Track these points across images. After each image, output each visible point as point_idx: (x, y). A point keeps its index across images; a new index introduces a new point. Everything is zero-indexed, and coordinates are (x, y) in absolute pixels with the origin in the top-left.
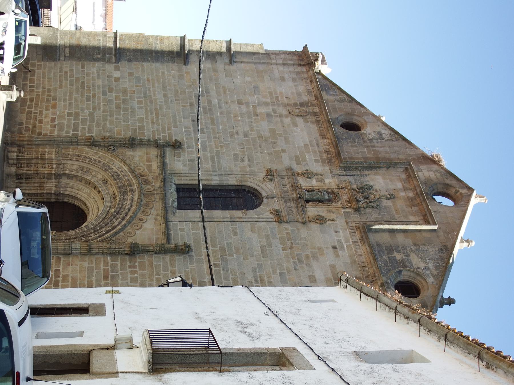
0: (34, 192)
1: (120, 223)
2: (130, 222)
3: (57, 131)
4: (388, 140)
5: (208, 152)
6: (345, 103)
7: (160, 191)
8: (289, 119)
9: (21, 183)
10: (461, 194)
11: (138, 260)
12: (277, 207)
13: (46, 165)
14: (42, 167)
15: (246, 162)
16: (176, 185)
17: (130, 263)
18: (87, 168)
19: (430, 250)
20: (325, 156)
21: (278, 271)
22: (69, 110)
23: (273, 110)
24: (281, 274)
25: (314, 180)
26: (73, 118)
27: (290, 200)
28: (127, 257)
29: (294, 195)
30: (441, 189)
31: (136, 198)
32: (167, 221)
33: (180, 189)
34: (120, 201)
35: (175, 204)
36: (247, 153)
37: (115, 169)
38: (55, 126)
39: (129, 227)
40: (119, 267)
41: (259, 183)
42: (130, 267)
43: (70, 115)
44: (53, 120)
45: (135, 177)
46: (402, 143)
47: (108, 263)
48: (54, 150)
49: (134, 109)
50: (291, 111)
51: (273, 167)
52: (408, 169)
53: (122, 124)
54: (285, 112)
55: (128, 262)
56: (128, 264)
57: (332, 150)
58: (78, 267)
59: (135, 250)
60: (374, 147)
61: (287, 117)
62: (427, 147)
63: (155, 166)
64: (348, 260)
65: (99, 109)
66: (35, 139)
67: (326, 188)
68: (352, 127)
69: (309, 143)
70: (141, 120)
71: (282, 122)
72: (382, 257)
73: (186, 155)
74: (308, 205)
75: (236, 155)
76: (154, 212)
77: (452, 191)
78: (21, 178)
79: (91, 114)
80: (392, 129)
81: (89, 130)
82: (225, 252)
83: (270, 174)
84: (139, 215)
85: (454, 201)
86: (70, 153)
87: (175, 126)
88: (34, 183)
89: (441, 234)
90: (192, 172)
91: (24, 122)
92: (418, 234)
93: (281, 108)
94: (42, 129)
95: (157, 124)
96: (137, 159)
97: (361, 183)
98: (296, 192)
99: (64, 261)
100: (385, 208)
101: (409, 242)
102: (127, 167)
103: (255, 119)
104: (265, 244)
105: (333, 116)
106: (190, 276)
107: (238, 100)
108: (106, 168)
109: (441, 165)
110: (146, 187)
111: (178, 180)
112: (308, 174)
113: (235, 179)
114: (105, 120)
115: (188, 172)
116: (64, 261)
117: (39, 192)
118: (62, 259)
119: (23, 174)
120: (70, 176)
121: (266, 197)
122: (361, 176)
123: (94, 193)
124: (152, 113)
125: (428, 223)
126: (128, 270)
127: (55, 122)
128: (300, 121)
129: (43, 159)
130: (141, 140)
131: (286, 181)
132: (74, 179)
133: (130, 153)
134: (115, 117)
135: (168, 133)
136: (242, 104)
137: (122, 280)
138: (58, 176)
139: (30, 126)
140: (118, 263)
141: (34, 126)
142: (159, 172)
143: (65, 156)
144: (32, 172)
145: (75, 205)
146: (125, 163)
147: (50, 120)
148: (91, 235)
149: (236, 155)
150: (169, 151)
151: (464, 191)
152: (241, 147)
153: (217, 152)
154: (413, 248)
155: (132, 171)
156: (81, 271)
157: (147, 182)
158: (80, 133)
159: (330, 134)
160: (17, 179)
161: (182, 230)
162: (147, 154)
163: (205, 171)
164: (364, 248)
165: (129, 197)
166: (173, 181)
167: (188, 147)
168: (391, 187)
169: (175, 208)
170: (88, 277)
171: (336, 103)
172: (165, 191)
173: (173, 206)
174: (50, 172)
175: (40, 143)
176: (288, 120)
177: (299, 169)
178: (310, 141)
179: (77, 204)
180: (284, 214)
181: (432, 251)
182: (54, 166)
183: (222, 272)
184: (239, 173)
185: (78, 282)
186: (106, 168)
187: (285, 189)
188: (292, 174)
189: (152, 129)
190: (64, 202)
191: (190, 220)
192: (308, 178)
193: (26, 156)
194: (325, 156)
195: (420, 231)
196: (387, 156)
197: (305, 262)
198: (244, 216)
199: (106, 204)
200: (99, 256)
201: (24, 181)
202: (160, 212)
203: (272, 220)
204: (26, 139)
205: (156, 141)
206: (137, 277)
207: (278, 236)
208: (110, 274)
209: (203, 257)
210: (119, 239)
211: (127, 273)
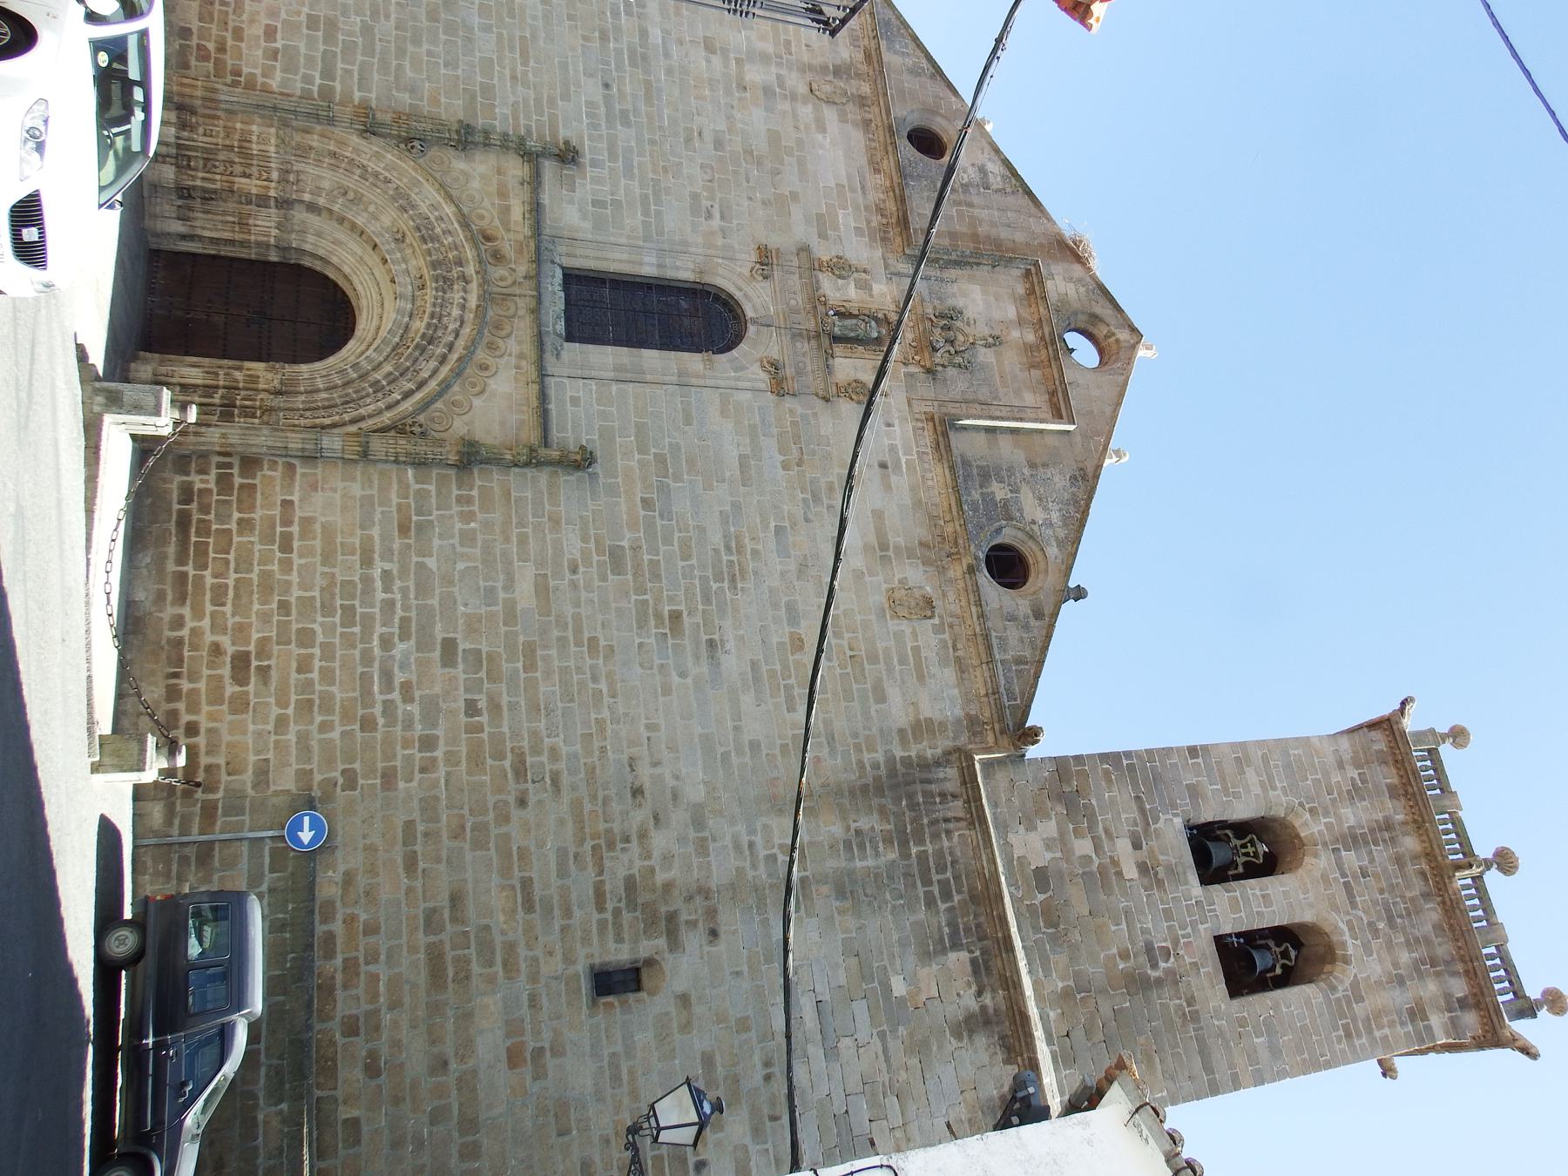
0: (226, 235)
1: (435, 372)
2: (458, 373)
3: (283, 71)
4: (997, 191)
5: (636, 183)
6: (924, 79)
7: (527, 289)
8: (810, 108)
9: (191, 209)
10: (1117, 341)
11: (478, 483)
12: (774, 353)
13: (254, 170)
14: (245, 175)
15: (716, 222)
16: (563, 268)
17: (459, 488)
18: (356, 192)
19: (1056, 479)
20: (876, 220)
21: (772, 524)
22: (311, 7)
23: (779, 77)
24: (779, 531)
25: (852, 285)
26: (320, 34)
27: (801, 335)
28: (452, 472)
29: (811, 325)
30: (1082, 321)
31: (473, 302)
32: (542, 375)
33: (573, 279)
34: (434, 305)
35: (561, 326)
36: (719, 195)
37: (424, 208)
38: (274, 55)
39: (456, 388)
40: (433, 500)
41: (740, 283)
42: (459, 500)
43: (313, 22)
44: (270, 33)
45: (472, 240)
46: (1024, 201)
47: (408, 486)
48: (273, 130)
49: (470, 29)
50: (815, 86)
51: (774, 241)
52: (1033, 277)
53: (443, 71)
54: (802, 89)
55: (454, 487)
56: (455, 492)
57: (891, 206)
58: (338, 496)
59: (471, 458)
60: (970, 205)
61: (805, 102)
62: (1067, 217)
63: (518, 211)
64: (908, 501)
65: (387, 17)
66: (223, 97)
67: (874, 307)
68: (927, 142)
69: (845, 183)
70: (487, 65)
71: (795, 115)
72: (969, 494)
73: (587, 185)
74: (839, 349)
75: (695, 197)
76: (512, 346)
77: (1100, 332)
78: (190, 196)
79: (367, 30)
80: (1007, 164)
81: (361, 79)
82: (666, 468)
83: (766, 260)
84: (481, 355)
85: (1101, 352)
86: (315, 144)
87: (566, 96)
88: (224, 213)
89: (1078, 439)
90: (600, 238)
91: (195, 30)
92: (1036, 437)
93: (794, 75)
94: (240, 58)
95: (526, 84)
96: (476, 184)
97: (940, 299)
98: (815, 317)
99: (303, 475)
100: (983, 367)
101: (1020, 456)
102: (453, 208)
103: (740, 99)
104: (748, 451)
105: (898, 111)
106: (592, 532)
107: (705, 38)
108: (404, 202)
109: (1089, 269)
110: (497, 272)
111: (568, 255)
112: (840, 268)
113: (691, 266)
114: (401, 52)
115: (590, 237)
116: (303, 475)
117: (238, 237)
118: (299, 470)
119: (194, 188)
120: (312, 208)
121: (754, 321)
122: (942, 280)
123: (373, 259)
124: (512, 49)
125: (1058, 416)
126: (456, 509)
127: (275, 41)
128: (830, 114)
129: (245, 153)
130: (486, 133)
131: (795, 282)
132: (325, 214)
133: (459, 164)
134: (425, 46)
135: (550, 115)
136: (713, 52)
137: (441, 537)
138: (284, 204)
139: (211, 46)
140: (432, 488)
141: (221, 49)
142: (528, 232)
143: (303, 152)
144: (218, 186)
145: (327, 277)
146: (449, 197)
147: (261, 32)
148: (368, 400)
149: (695, 197)
150: (549, 167)
151: (1124, 335)
152: (707, 177)
153: (656, 182)
154: (1026, 471)
155: (465, 223)
156: (344, 509)
157: (498, 257)
158: (338, 86)
159: (888, 165)
160: (180, 197)
161: (575, 401)
162: (499, 173)
163: (629, 237)
164: (939, 470)
165: (457, 297)
166: (557, 260)
167: (594, 164)
168: (997, 315)
169: (560, 336)
170: (363, 528)
171: (906, 77)
172: (538, 288)
173: (555, 333)
174: (263, 192)
175: (236, 108)
176: (806, 111)
177: (823, 252)
178: (849, 177)
179: (331, 276)
180: (789, 372)
181: (1060, 481)
182: (275, 175)
183: (659, 522)
184: (700, 251)
185: (338, 540)
186: (404, 202)
187: (793, 302)
188: (813, 266)
189: (512, 99)
190: (299, 266)
191: (593, 374)
192: (840, 277)
193: (201, 140)
194: (876, 220)
195: (1041, 431)
196: (994, 232)
197: (825, 501)
198: (708, 373)
199: (403, 304)
200: (388, 466)
201: (197, 204)
202: (529, 349)
203: (763, 386)
204: (199, 93)
205: (522, 141)
206: (474, 530)
207: (775, 431)
208: (414, 518)
209: (619, 480)
210: (432, 420)
211: (451, 517)
